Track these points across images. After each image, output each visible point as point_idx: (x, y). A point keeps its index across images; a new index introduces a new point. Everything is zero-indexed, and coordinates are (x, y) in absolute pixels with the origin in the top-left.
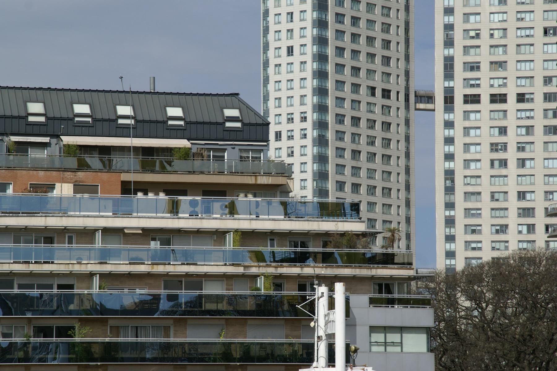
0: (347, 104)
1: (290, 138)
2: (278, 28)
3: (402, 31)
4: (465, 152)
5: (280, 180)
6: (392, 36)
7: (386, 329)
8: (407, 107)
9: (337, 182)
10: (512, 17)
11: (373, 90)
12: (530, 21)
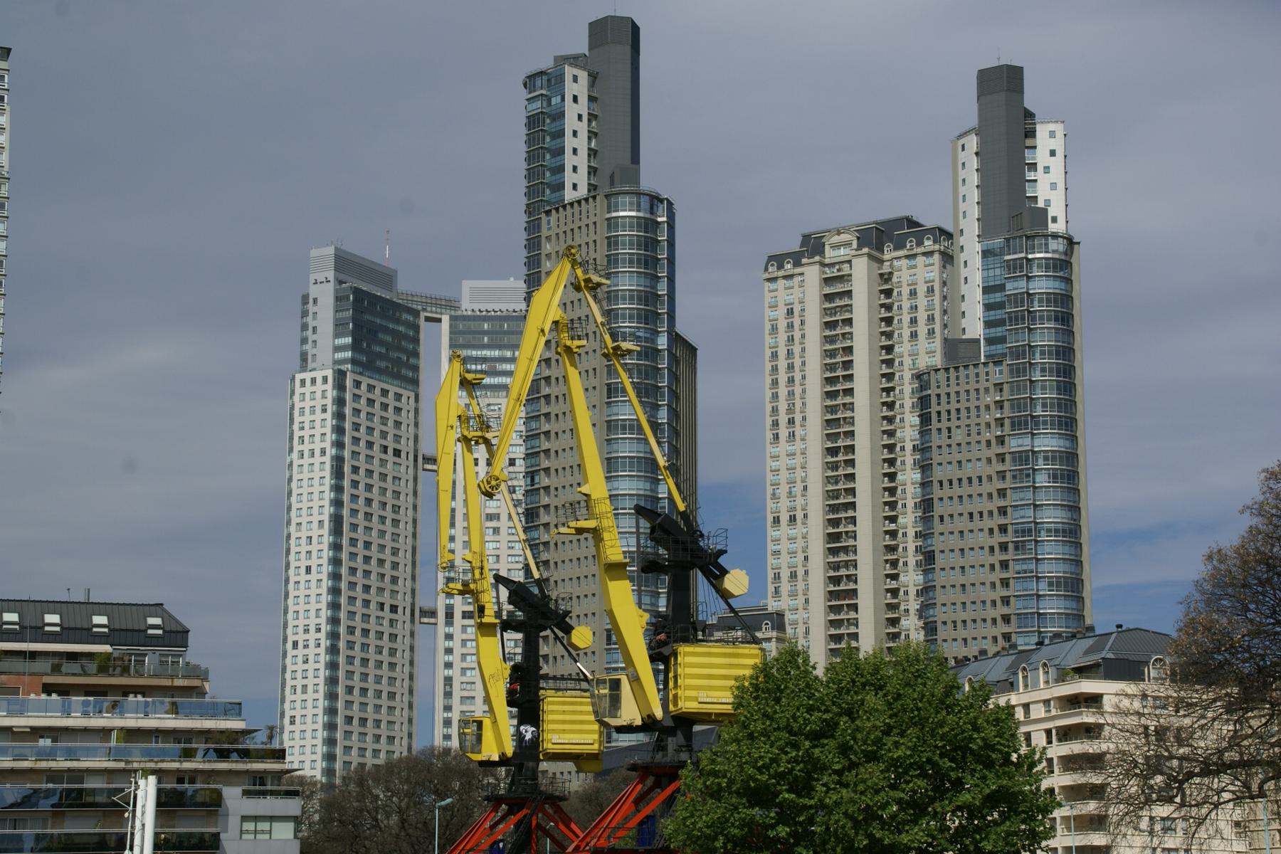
0: (358, 617)
1: (306, 647)
2: (298, 549)
3: (409, 555)
4: (462, 661)
5: (196, 683)
6: (400, 558)
7: (256, 819)
8: (412, 621)
9: (347, 686)
10: (504, 545)
11: (382, 606)
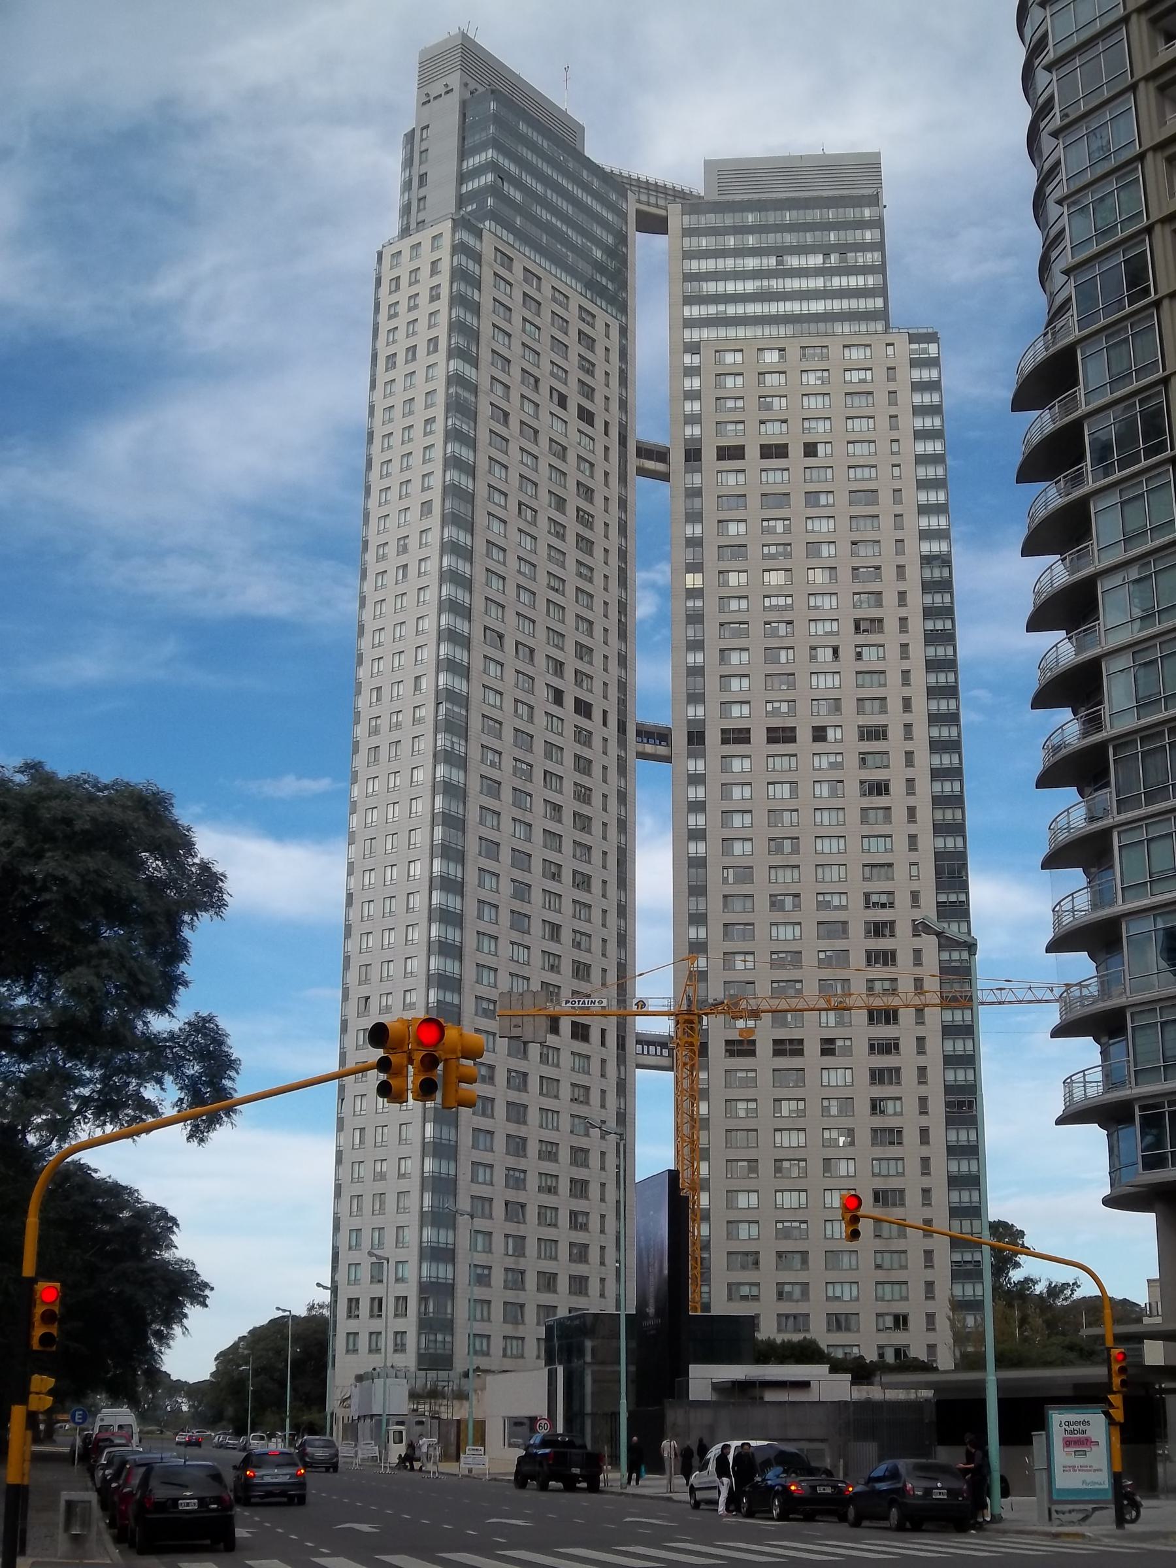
12: (851, 1300)
